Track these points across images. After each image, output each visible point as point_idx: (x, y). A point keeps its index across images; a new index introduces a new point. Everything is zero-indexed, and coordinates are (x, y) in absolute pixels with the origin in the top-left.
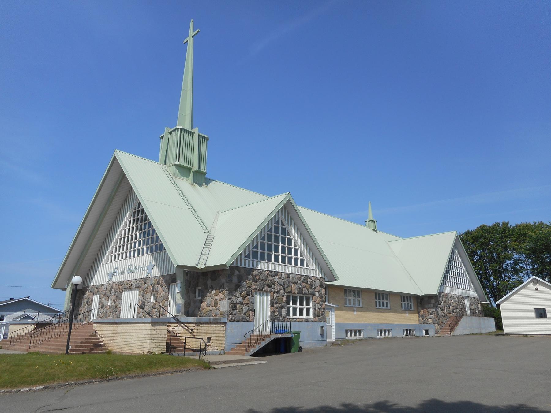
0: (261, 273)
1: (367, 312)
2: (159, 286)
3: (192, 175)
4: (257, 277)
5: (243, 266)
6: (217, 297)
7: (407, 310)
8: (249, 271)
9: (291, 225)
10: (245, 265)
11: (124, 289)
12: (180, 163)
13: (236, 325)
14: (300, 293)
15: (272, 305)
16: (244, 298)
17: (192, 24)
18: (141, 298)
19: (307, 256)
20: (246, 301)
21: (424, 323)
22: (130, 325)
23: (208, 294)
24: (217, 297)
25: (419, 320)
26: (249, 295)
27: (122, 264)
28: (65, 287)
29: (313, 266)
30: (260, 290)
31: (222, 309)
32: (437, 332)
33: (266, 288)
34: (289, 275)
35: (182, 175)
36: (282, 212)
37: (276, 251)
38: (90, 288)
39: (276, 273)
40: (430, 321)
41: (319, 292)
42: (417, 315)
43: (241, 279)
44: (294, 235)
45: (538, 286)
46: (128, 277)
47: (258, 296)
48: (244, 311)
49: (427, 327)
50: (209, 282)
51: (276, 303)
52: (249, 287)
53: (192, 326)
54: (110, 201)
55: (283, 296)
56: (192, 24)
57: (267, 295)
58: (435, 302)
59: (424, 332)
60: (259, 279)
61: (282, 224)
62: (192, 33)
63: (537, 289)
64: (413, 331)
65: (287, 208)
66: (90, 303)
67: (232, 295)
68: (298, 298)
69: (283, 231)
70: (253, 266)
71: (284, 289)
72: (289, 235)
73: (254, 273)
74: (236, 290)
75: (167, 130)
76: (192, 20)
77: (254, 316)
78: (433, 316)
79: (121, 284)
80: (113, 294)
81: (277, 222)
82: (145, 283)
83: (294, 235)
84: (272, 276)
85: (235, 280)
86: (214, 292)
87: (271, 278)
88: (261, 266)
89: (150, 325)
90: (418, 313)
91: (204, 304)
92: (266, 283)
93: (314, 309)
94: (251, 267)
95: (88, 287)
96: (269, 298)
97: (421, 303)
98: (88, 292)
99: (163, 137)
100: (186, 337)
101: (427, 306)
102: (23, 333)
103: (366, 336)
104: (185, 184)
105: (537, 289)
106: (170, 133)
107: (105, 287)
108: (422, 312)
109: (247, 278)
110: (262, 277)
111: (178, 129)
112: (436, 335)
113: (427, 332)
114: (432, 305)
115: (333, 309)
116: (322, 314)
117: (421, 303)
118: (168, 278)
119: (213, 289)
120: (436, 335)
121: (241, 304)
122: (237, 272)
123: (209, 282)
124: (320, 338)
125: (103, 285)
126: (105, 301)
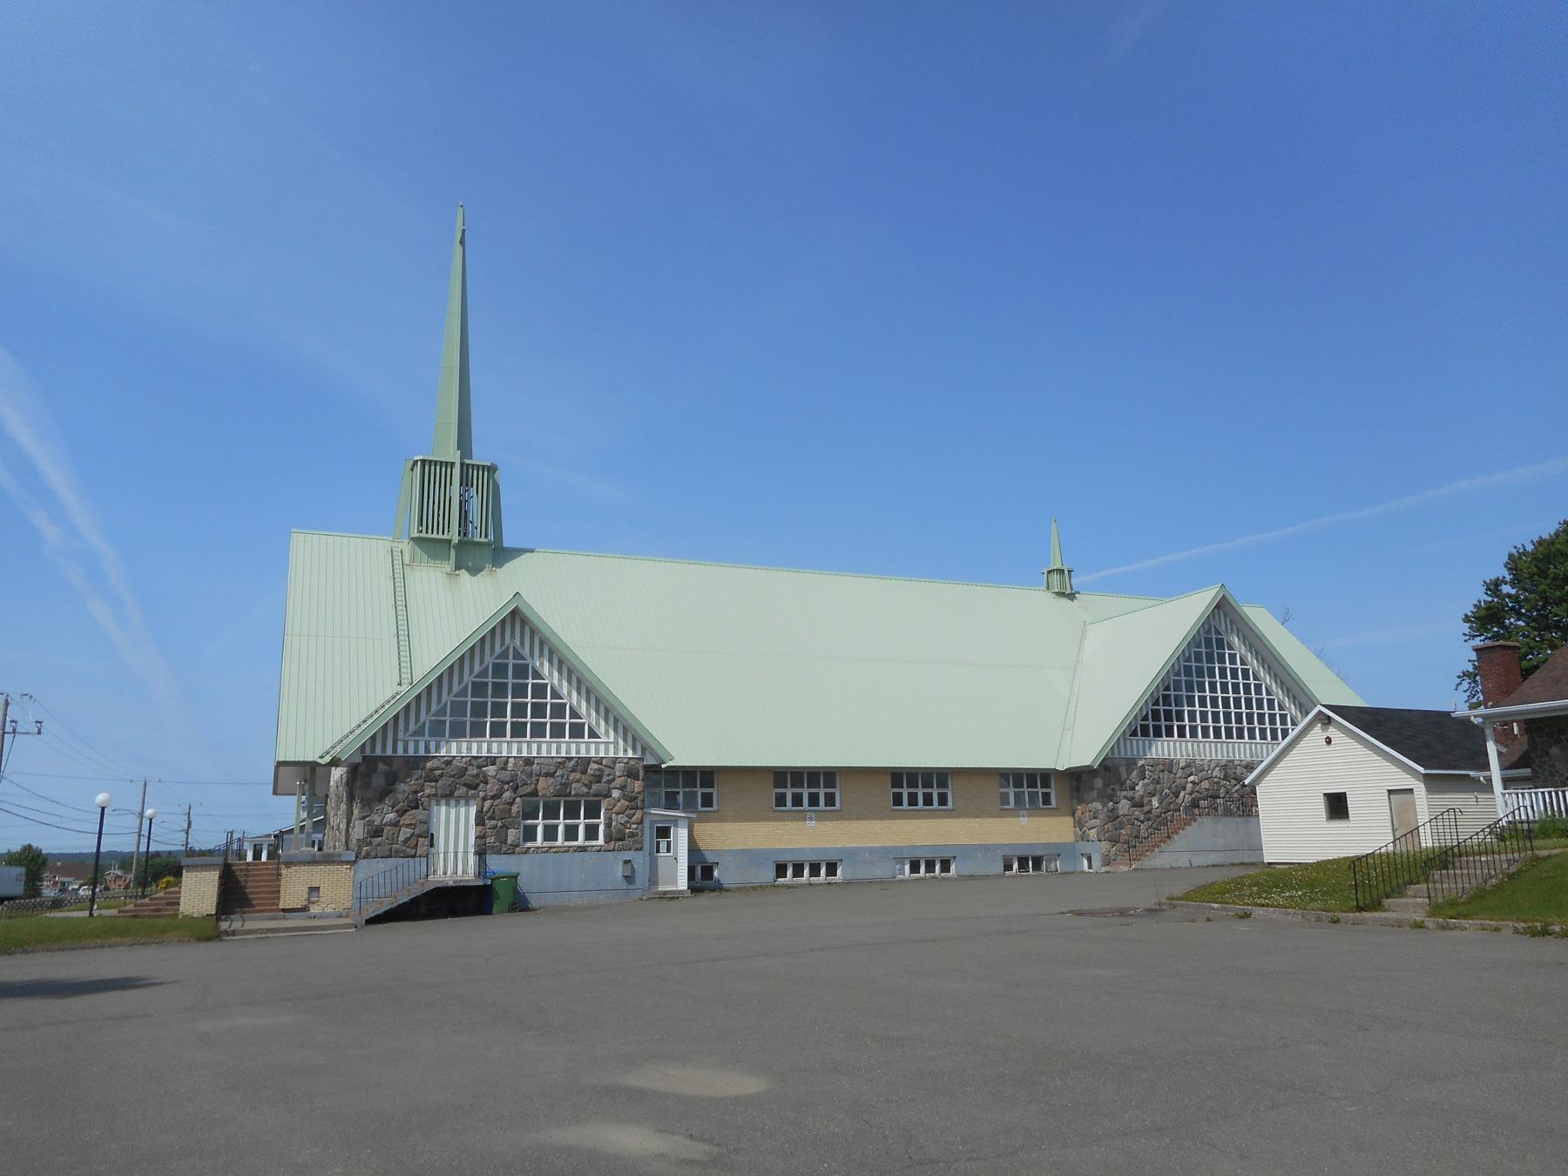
0: (448, 763)
1: (858, 819)
4: (438, 772)
5: (400, 752)
7: (1002, 809)
8: (416, 762)
9: (541, 655)
10: (406, 750)
13: (380, 865)
14: (564, 790)
15: (480, 821)
16: (402, 813)
19: (588, 716)
20: (406, 819)
26: (417, 807)
29: (607, 734)
30: (448, 796)
32: (1107, 861)
33: (462, 790)
34: (529, 761)
36: (503, 634)
37: (1212, 675)
39: (492, 761)
41: (622, 788)
42: (1071, 819)
43: (392, 779)
44: (1240, 649)
45: (1332, 732)
47: (443, 809)
48: (401, 838)
51: (491, 818)
52: (416, 792)
55: (511, 804)
57: (467, 804)
58: (1106, 785)
60: (442, 775)
61: (1218, 633)
63: (1329, 741)
64: (1049, 862)
65: (1222, 607)
67: (371, 810)
68: (1489, 732)
69: (521, 671)
70: (427, 749)
71: (515, 789)
72: (1230, 648)
73: (429, 765)
74: (381, 800)
77: (432, 845)
78: (1097, 822)
81: (1209, 632)
83: (551, 676)
84: (479, 767)
85: (378, 781)
87: (475, 771)
88: (449, 751)
92: (463, 782)
93: (608, 826)
94: (422, 752)
96: (473, 810)
103: (849, 877)
104: (1065, 602)
105: (1329, 741)
108: (1078, 813)
109: (409, 776)
110: (450, 770)
112: (1104, 869)
114: (1095, 794)
115: (680, 823)
116: (632, 835)
117: (1077, 790)
121: (396, 824)
122: (382, 767)
124: (625, 885)
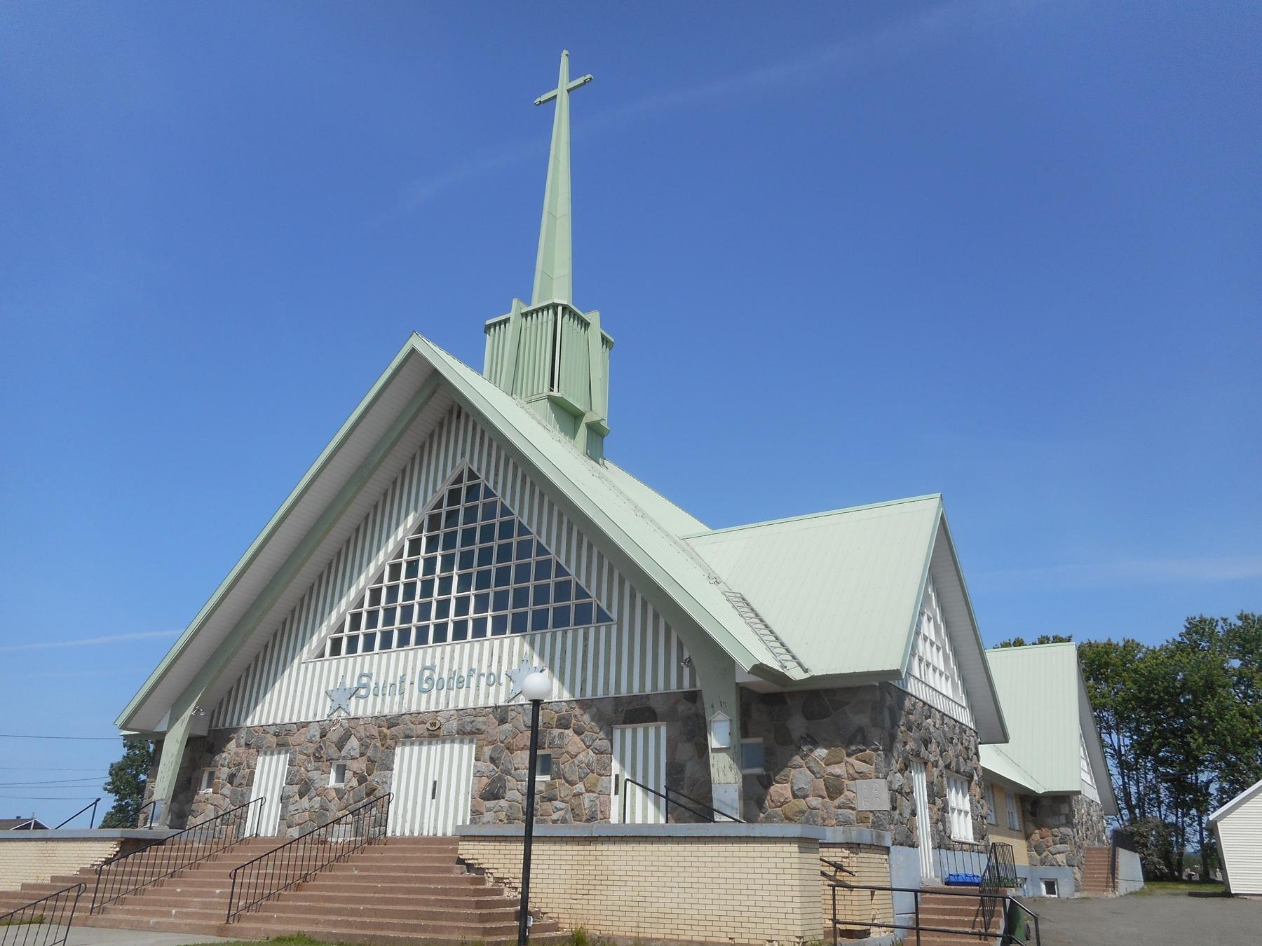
2: (570, 732)
3: (582, 430)
6: (838, 770)
11: (408, 738)
12: (555, 393)
17: (564, 62)
18: (487, 767)
21: (1043, 863)
22: (677, 848)
23: (797, 759)
24: (838, 770)
25: (1030, 857)
27: (350, 667)
28: (161, 728)
31: (863, 806)
35: (562, 429)
38: (243, 734)
40: (1061, 858)
46: (417, 702)
49: (1051, 873)
50: (798, 725)
53: (836, 855)
54: (360, 475)
56: (564, 62)
59: (1043, 887)
62: (564, 82)
66: (241, 779)
75: (517, 307)
76: (565, 52)
79: (392, 722)
80: (356, 753)
82: (503, 721)
86: (821, 752)
89: (794, 848)
90: (1027, 837)
91: (775, 789)
95: (236, 730)
97: (1033, 814)
98: (232, 745)
99: (506, 321)
100: (916, 892)
101: (1050, 821)
102: (70, 870)
106: (525, 315)
107: (315, 731)
111: (555, 306)
112: (1077, 895)
113: (1051, 887)
118: (609, 709)
119: (815, 744)
120: (1077, 895)
123: (798, 725)
125: (305, 725)
126: (315, 775)
